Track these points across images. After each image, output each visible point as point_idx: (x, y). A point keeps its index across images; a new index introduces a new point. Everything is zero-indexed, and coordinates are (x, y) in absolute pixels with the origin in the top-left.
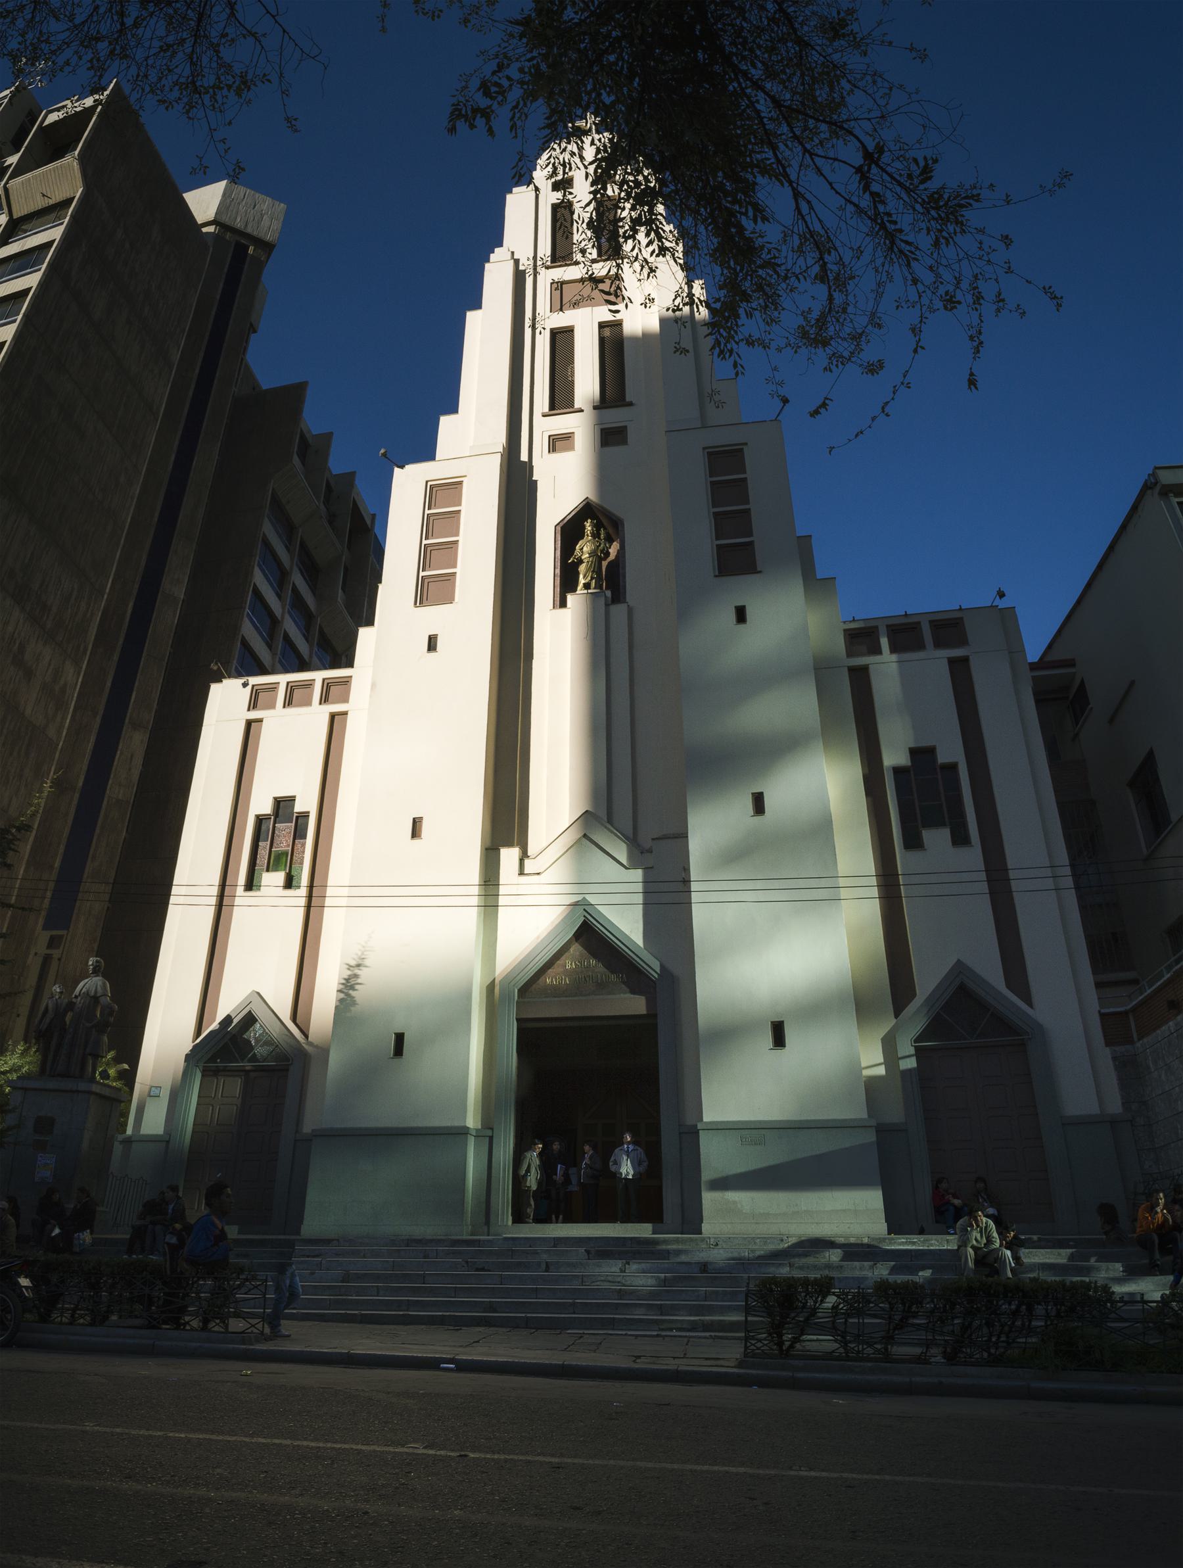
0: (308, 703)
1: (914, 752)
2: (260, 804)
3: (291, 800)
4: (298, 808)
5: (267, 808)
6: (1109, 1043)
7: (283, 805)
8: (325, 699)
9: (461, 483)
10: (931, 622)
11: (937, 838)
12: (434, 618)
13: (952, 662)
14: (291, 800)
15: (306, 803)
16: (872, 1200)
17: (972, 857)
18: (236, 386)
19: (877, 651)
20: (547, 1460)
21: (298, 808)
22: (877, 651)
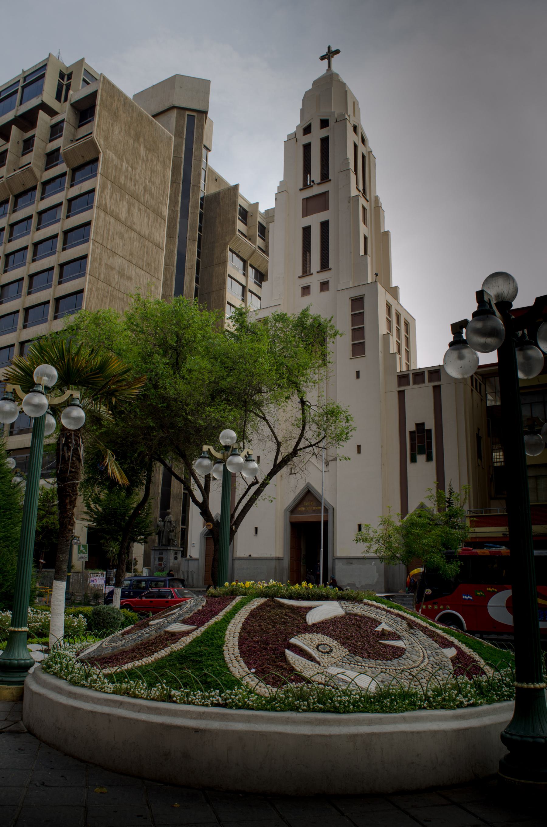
0: (424, 382)
1: (417, 425)
2: (410, 427)
3: (423, 424)
4: (426, 427)
5: (413, 428)
6: (34, 557)
7: (420, 426)
8: (430, 381)
9: (363, 298)
10: (428, 371)
11: (422, 458)
12: (359, 363)
13: (434, 387)
14: (423, 424)
15: (430, 425)
16: (56, 583)
17: (433, 464)
18: (365, 222)
19: (408, 384)
20: (432, 629)
21: (426, 427)
22: (408, 384)
